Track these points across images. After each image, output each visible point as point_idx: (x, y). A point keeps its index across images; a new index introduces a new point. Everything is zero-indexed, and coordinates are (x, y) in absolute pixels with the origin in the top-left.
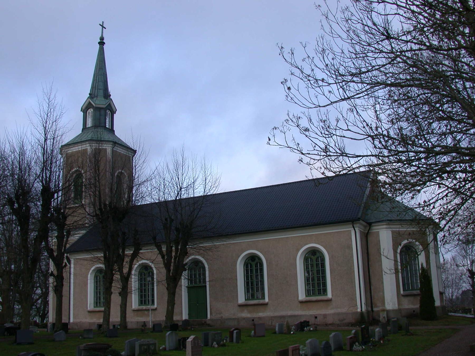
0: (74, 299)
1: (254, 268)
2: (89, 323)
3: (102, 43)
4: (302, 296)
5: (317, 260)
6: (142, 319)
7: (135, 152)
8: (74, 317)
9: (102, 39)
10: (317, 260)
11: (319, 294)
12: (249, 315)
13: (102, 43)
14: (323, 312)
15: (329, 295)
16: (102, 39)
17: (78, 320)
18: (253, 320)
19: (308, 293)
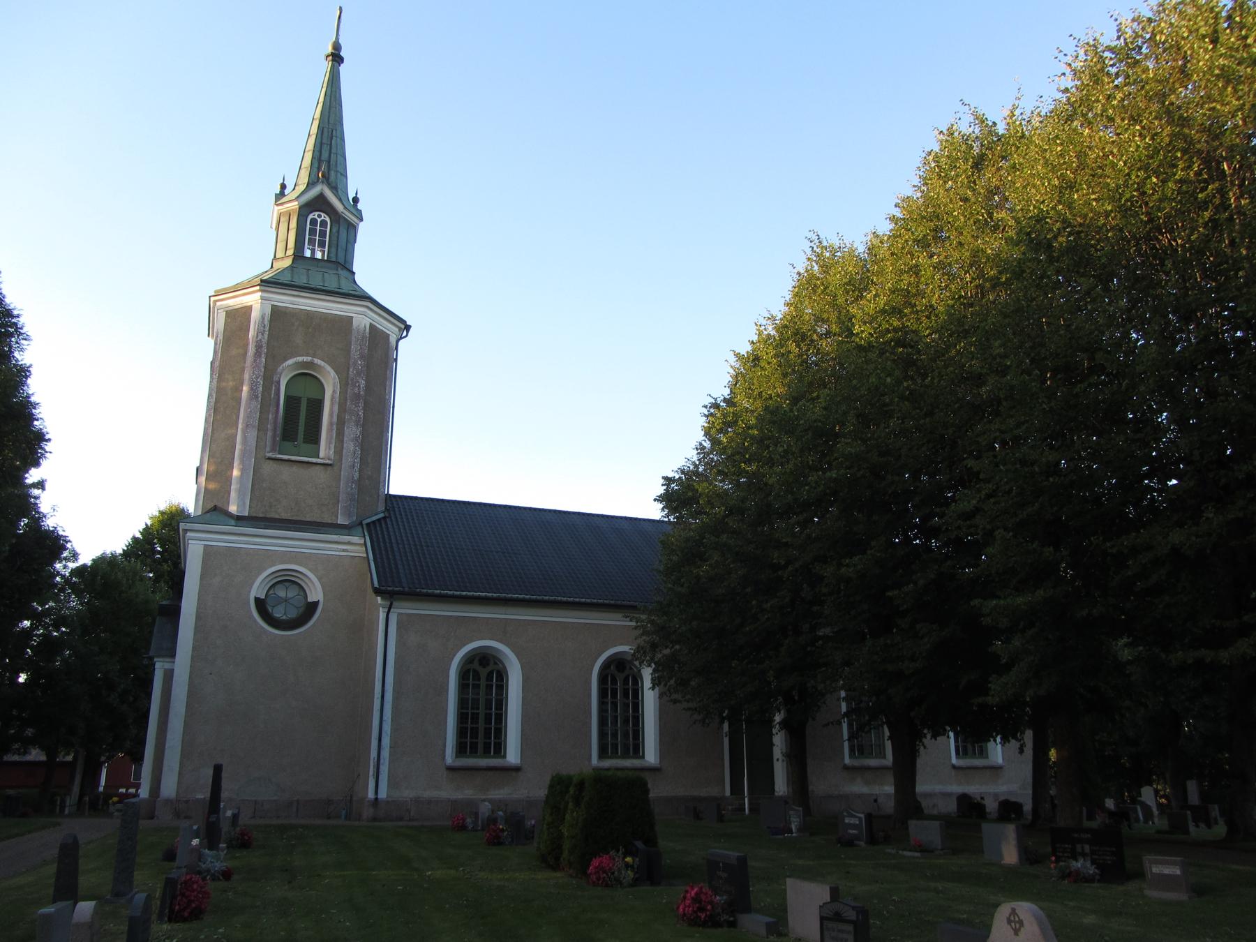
0: (590, 703)
1: (483, 683)
2: (454, 803)
3: (336, 57)
4: (450, 757)
5: (626, 680)
6: (467, 793)
7: (408, 328)
8: (392, 784)
9: (337, 47)
10: (626, 680)
11: (486, 753)
12: (865, 790)
13: (336, 57)
14: (499, 794)
15: (513, 755)
16: (337, 47)
17: (407, 794)
18: (876, 801)
19: (461, 750)
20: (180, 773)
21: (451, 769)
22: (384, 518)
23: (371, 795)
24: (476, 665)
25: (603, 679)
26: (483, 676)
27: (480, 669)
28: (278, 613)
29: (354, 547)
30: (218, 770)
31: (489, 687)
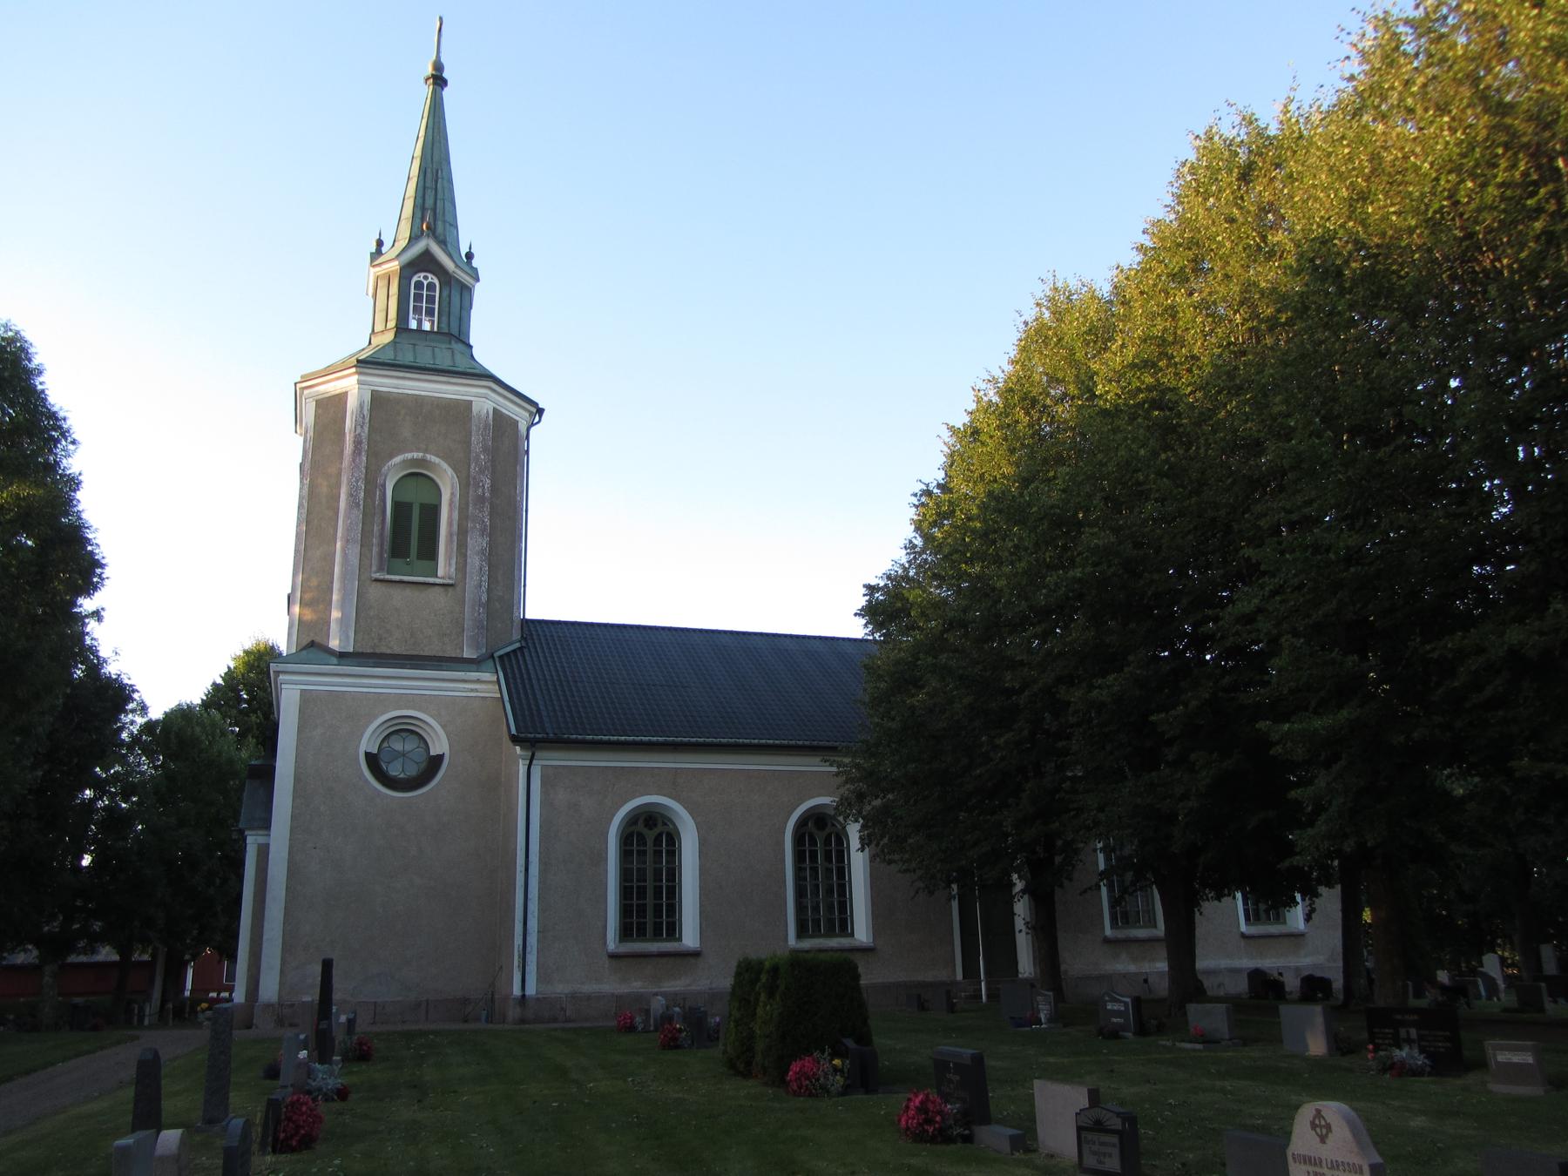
4: (612, 944)
8: (543, 977)
10: (827, 841)
19: (626, 932)
20: (282, 972)
21: (614, 956)
22: (521, 648)
23: (517, 991)
24: (640, 827)
25: (799, 839)
26: (649, 840)
27: (645, 831)
28: (395, 770)
29: (484, 686)
30: (327, 966)
31: (658, 853)
